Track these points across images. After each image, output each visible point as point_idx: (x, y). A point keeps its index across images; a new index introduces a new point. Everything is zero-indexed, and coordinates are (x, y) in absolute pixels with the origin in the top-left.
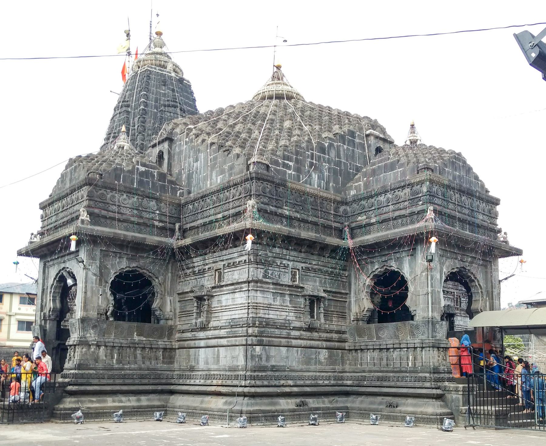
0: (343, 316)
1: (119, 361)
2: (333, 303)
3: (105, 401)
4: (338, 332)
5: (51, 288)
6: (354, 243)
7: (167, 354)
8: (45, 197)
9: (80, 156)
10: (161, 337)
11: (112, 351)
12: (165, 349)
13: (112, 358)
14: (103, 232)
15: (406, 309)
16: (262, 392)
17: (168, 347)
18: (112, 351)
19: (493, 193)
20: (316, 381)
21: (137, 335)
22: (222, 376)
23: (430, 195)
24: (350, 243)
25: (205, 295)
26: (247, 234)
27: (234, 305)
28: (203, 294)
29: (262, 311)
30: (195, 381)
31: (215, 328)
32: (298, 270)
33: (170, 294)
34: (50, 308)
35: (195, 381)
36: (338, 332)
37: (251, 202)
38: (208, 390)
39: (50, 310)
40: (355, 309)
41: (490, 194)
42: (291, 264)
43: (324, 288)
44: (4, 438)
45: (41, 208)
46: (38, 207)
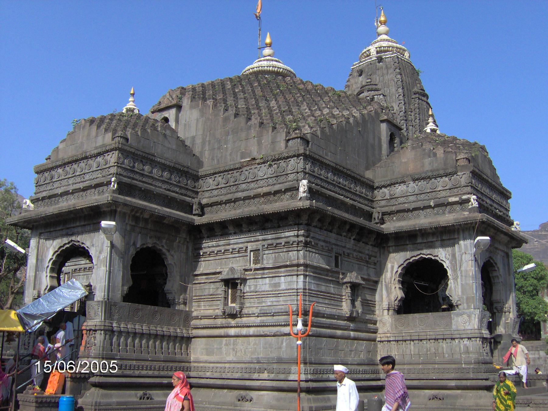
3: (111, 396)
5: (49, 262)
8: (42, 161)
9: (455, 139)
14: (138, 204)
15: (446, 299)
16: (149, 383)
19: (506, 183)
20: (375, 375)
22: (243, 369)
23: (118, 167)
24: (198, 220)
25: (238, 279)
27: (290, 289)
28: (236, 276)
30: (259, 376)
31: (249, 315)
32: (341, 255)
34: (47, 286)
35: (259, 376)
37: (305, 182)
38: (247, 384)
39: (46, 289)
45: (37, 173)
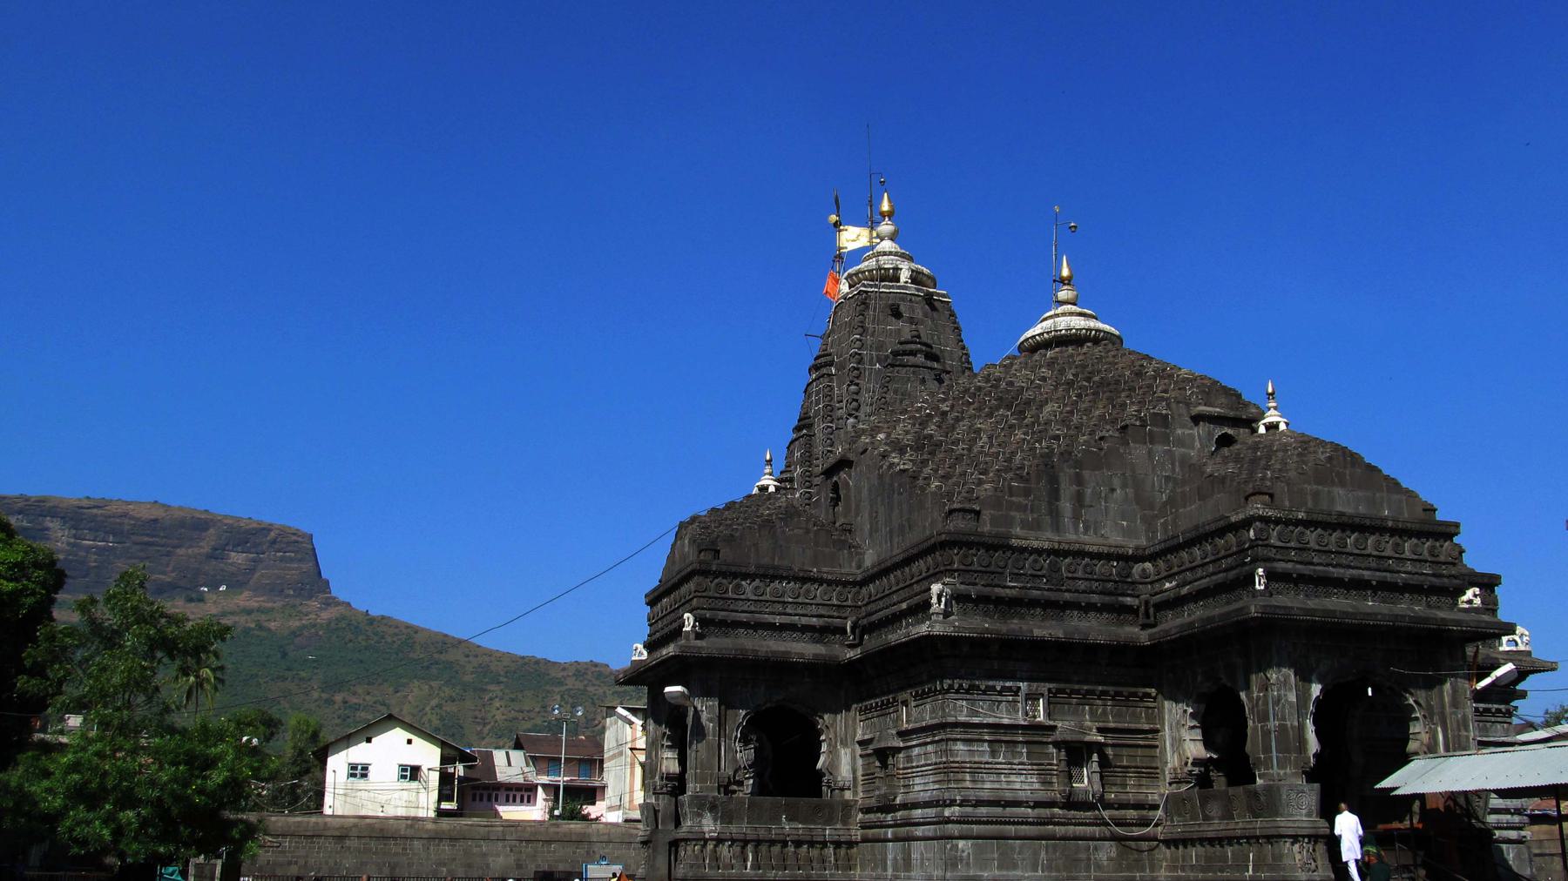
0: (1151, 773)
1: (756, 866)
2: (1125, 751)
4: (1138, 806)
6: (1151, 637)
7: (843, 851)
8: (652, 581)
10: (829, 821)
11: (743, 848)
12: (838, 844)
13: (745, 860)
17: (843, 839)
18: (743, 848)
21: (789, 819)
26: (1473, 585)
29: (917, 780)
33: (844, 744)
36: (1138, 806)
40: (1172, 761)
41: (1439, 516)
42: (1023, 685)
43: (1101, 725)
44: (1362, 866)
46: (644, 600)
